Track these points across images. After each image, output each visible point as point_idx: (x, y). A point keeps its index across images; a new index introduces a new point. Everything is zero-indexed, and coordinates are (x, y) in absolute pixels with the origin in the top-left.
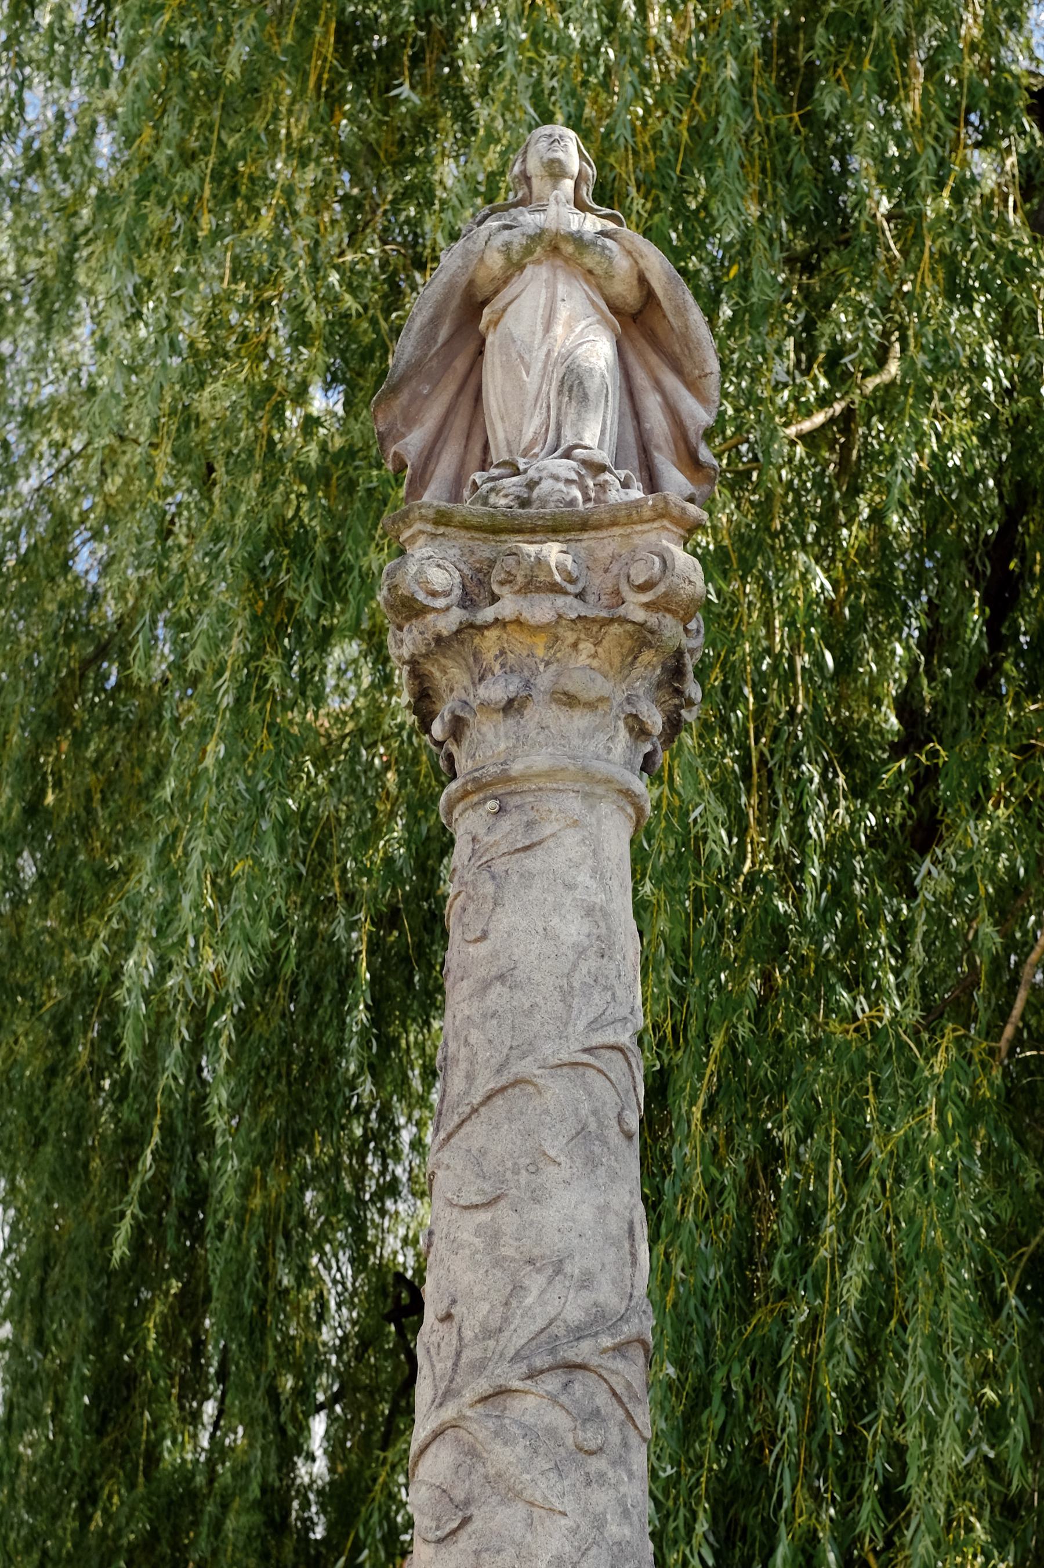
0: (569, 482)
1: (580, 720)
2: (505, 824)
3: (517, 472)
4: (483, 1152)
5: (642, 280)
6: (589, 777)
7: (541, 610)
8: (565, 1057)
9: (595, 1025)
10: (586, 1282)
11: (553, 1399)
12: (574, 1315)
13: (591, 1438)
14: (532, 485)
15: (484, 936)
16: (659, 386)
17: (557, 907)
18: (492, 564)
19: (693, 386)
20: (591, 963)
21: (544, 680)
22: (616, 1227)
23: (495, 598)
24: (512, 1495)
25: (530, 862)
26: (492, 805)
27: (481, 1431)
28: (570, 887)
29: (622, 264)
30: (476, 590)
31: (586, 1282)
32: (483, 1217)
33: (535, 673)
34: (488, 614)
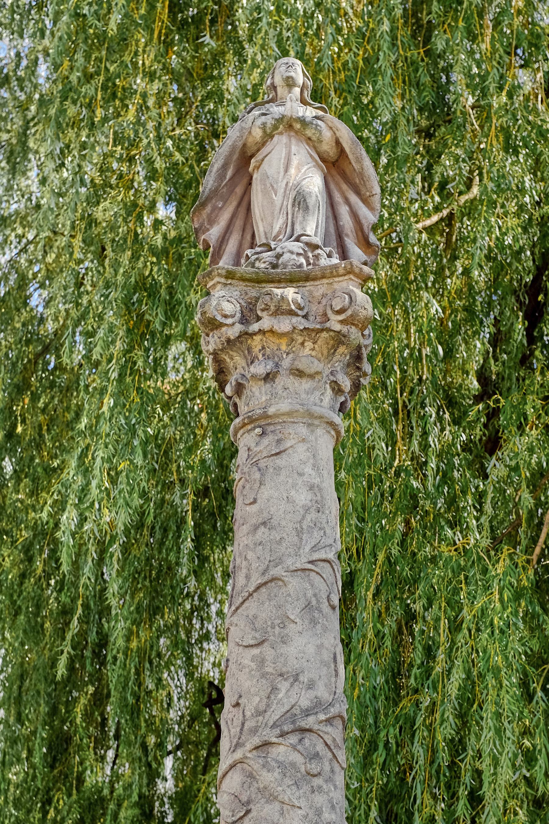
0: (299, 254)
1: (306, 384)
2: (266, 441)
3: (270, 249)
4: (255, 617)
5: (338, 143)
6: (311, 415)
7: (284, 325)
8: (299, 566)
9: (314, 549)
10: (311, 686)
11: (294, 747)
12: (305, 703)
13: (314, 768)
14: (278, 256)
15: (255, 501)
16: (347, 202)
17: (294, 486)
18: (257, 299)
19: (366, 201)
20: (312, 515)
21: (286, 363)
22: (327, 656)
23: (259, 319)
24: (272, 798)
25: (279, 461)
26: (258, 430)
27: (255, 765)
28: (301, 475)
29: (327, 134)
30: (248, 314)
31: (311, 686)
32: (256, 651)
33: (281, 359)
34: (255, 327)
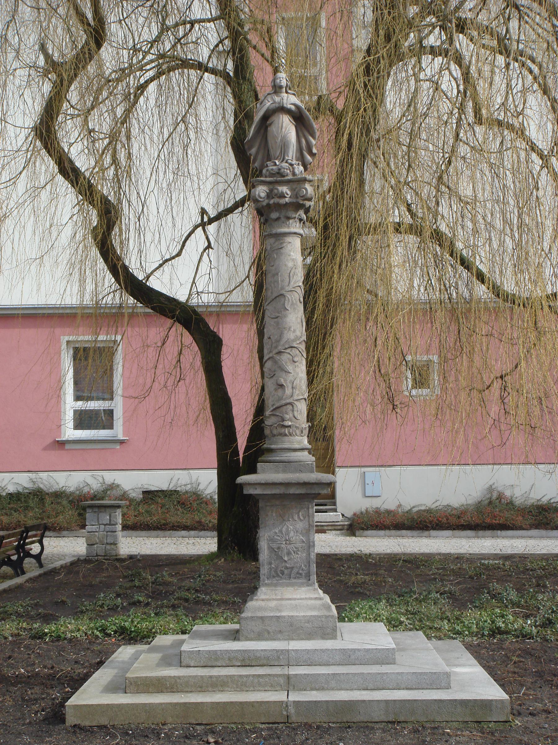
32: (276, 320)
